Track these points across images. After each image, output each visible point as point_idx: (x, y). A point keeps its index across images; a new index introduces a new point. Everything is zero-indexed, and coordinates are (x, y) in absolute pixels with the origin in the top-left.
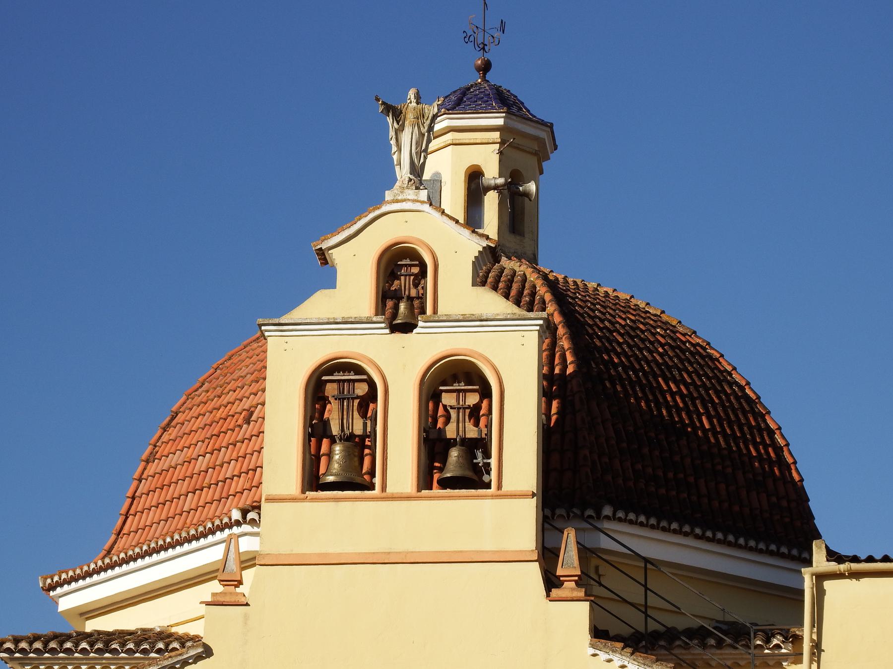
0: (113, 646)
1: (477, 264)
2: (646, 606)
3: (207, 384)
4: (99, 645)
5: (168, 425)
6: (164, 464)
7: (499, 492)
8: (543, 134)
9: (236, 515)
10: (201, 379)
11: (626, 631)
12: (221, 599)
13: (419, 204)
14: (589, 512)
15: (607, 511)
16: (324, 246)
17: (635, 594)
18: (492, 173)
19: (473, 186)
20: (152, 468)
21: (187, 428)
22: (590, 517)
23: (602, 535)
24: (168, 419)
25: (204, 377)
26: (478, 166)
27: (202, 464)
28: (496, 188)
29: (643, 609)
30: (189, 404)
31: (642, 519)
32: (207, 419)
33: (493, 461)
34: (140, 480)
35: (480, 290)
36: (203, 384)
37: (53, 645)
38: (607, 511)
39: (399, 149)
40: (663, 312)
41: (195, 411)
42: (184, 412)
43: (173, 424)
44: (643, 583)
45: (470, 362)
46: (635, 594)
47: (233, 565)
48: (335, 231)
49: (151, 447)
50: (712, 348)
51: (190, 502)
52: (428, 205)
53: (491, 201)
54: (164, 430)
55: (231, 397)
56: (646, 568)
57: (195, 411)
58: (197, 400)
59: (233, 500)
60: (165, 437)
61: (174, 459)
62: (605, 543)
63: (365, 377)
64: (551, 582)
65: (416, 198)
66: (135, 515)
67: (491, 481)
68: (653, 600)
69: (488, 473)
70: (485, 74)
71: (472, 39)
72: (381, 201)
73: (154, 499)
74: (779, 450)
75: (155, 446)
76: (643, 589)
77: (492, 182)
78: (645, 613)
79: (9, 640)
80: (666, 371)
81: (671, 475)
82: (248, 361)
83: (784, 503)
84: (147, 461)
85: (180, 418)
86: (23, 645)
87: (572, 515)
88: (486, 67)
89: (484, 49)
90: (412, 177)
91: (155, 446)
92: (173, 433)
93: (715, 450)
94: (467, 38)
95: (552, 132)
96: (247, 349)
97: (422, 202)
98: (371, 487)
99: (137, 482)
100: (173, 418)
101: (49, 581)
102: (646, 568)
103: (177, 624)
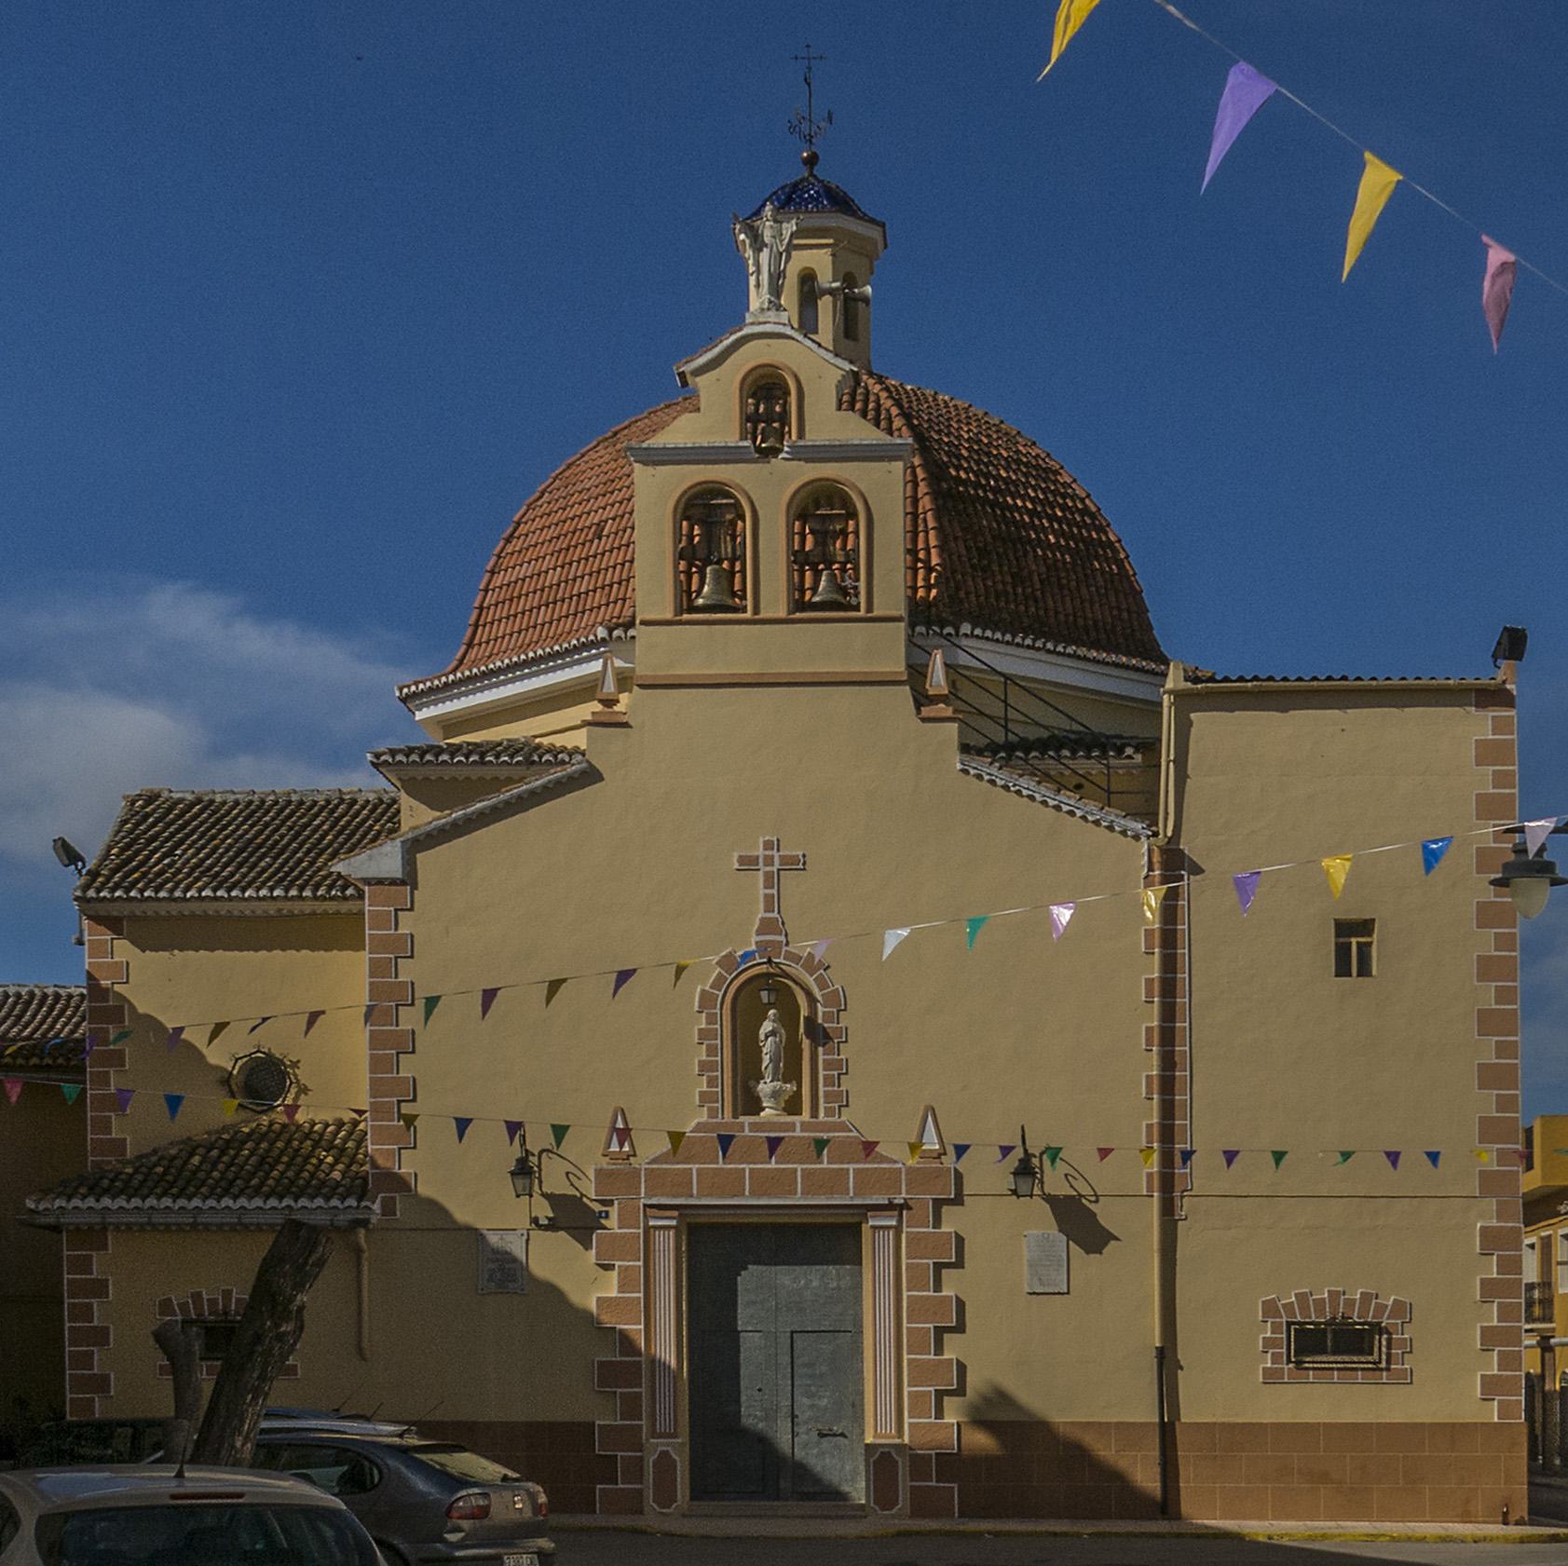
0: (487, 759)
1: (839, 386)
2: (1006, 719)
3: (547, 494)
4: (473, 758)
5: (512, 535)
6: (511, 576)
7: (869, 615)
8: (874, 233)
9: (601, 632)
10: (540, 489)
11: (983, 742)
12: (602, 719)
13: (781, 327)
14: (949, 630)
15: (966, 628)
16: (687, 368)
17: (997, 709)
18: (826, 278)
19: (806, 288)
20: (498, 581)
21: (532, 539)
22: (950, 634)
23: (960, 651)
24: (511, 529)
25: (543, 486)
26: (812, 269)
27: (553, 577)
28: (831, 292)
29: (1003, 722)
30: (530, 515)
31: (998, 635)
32: (552, 532)
33: (862, 585)
34: (486, 591)
35: (842, 413)
36: (543, 494)
37: (428, 757)
38: (966, 628)
39: (758, 271)
40: (1002, 422)
41: (538, 523)
42: (526, 523)
43: (516, 535)
44: (1003, 698)
45: (846, 493)
46: (997, 709)
47: (610, 686)
48: (696, 353)
49: (494, 558)
50: (1052, 460)
51: (543, 615)
52: (789, 328)
53: (825, 305)
54: (508, 541)
55: (577, 510)
56: (1006, 683)
57: (538, 523)
58: (539, 512)
59: (590, 615)
60: (509, 549)
61: (524, 571)
62: (964, 659)
63: (732, 501)
64: (921, 699)
65: (777, 320)
66: (484, 626)
67: (859, 603)
68: (1012, 714)
69: (857, 595)
70: (812, 169)
71: (797, 129)
72: (741, 323)
73: (503, 611)
74: (1120, 563)
75: (499, 557)
76: (1010, 701)
77: (827, 285)
78: (1005, 727)
79: (384, 753)
80: (1010, 487)
81: (1020, 590)
82: (589, 472)
83: (1125, 615)
84: (493, 572)
85: (523, 529)
86: (400, 757)
87: (931, 632)
88: (812, 161)
89: (810, 141)
90: (773, 299)
91: (499, 557)
92: (516, 545)
93: (1060, 565)
94: (792, 128)
95: (884, 233)
96: (585, 459)
97: (784, 325)
98: (744, 610)
99: (482, 593)
100: (515, 530)
101: (405, 690)
102: (1006, 683)
103: (541, 736)
